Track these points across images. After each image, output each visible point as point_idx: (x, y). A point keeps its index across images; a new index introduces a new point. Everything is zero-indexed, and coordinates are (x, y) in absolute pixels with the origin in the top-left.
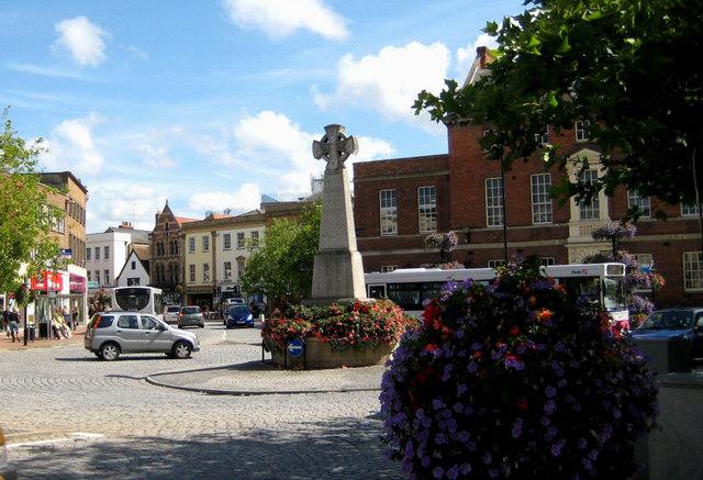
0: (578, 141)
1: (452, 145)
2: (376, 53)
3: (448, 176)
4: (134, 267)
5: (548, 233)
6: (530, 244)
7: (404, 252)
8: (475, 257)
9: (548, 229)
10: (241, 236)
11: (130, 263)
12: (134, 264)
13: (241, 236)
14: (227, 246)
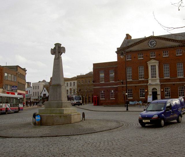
0: (151, 57)
1: (119, 58)
2: (118, 48)
3: (117, 67)
4: (45, 91)
5: (143, 82)
6: (138, 85)
7: (106, 87)
8: (124, 88)
9: (143, 81)
10: (71, 83)
11: (44, 90)
12: (45, 90)
13: (71, 83)
14: (67, 85)
